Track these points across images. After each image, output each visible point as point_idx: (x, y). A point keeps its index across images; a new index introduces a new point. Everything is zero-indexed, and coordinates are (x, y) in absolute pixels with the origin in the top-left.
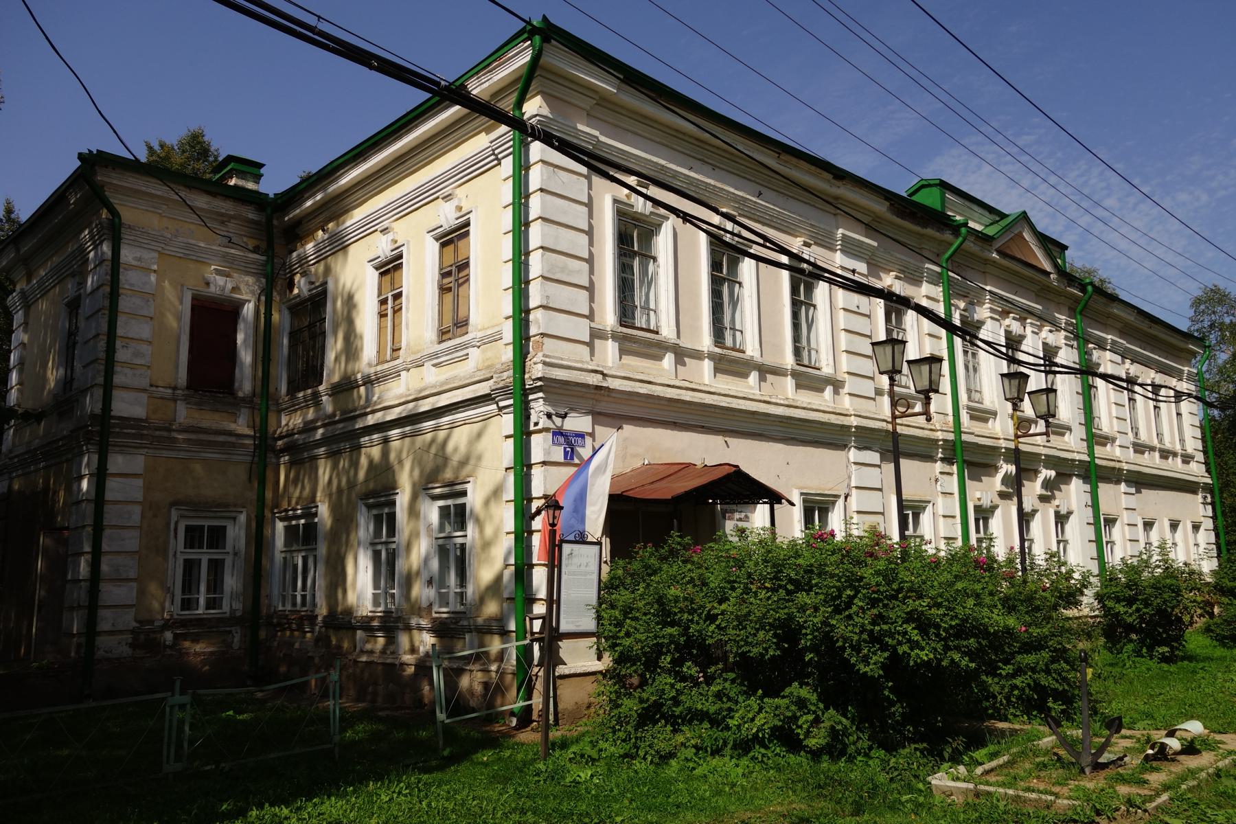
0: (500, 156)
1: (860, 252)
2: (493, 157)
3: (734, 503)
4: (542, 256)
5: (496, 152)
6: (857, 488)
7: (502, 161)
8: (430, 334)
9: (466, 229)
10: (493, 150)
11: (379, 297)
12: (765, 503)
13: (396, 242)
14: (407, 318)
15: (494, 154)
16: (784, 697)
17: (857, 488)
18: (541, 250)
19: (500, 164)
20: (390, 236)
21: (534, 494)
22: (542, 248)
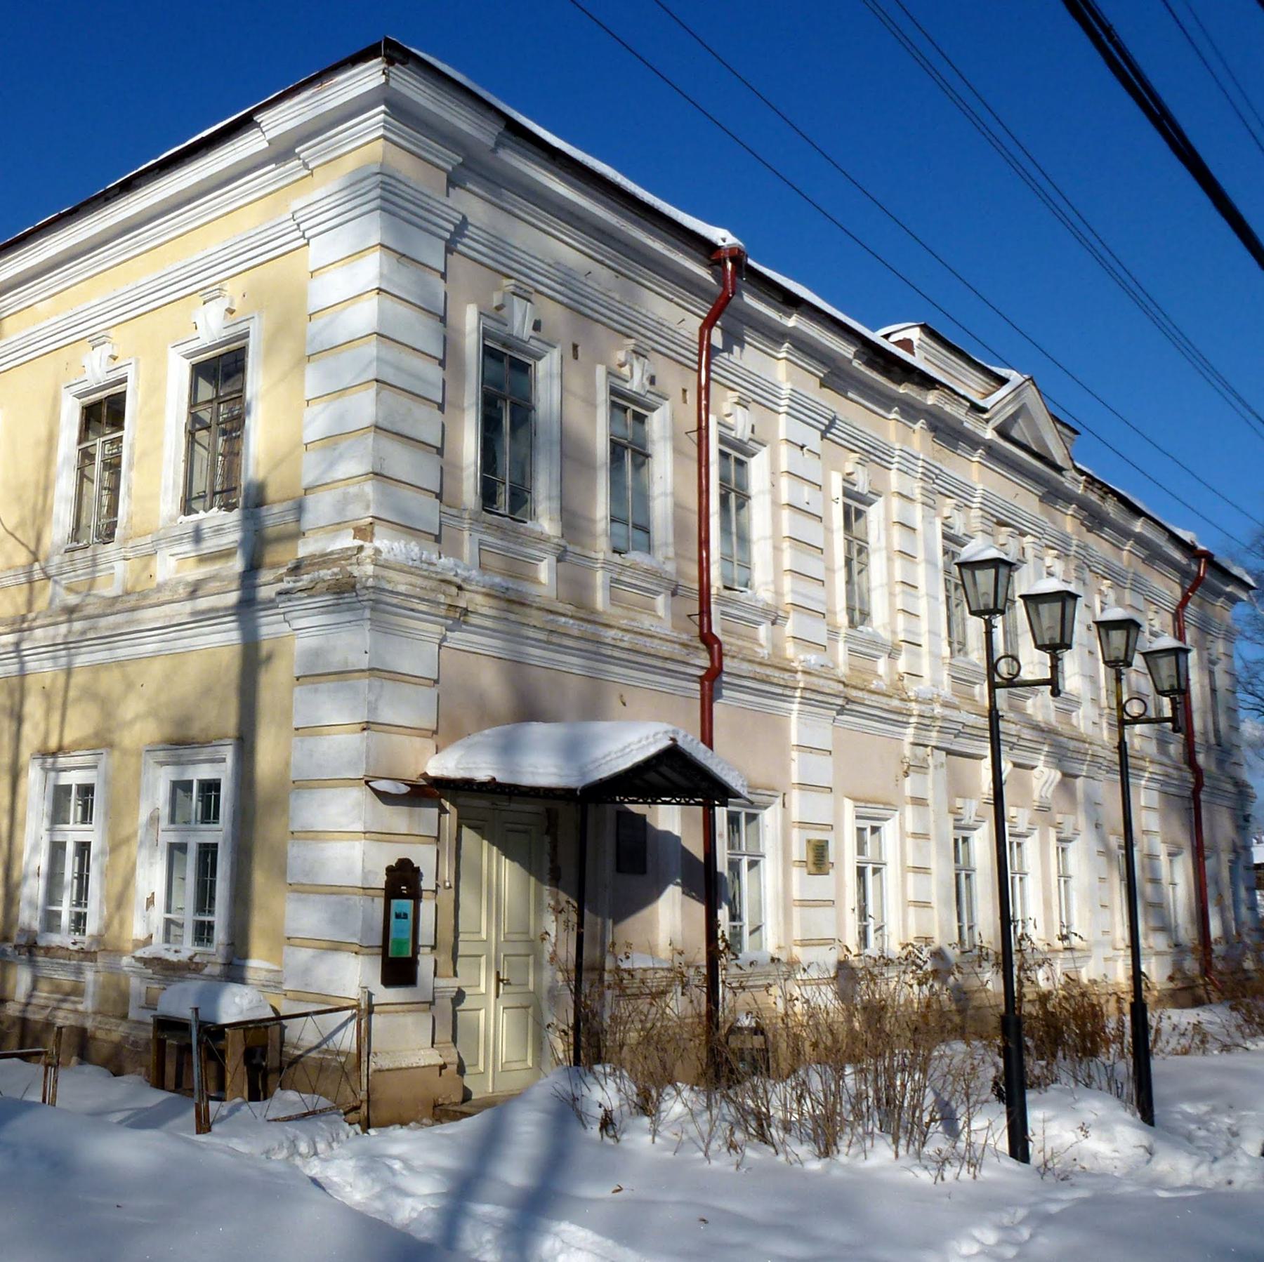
0: (308, 234)
1: (882, 459)
2: (298, 234)
3: (645, 802)
4: (378, 394)
5: (303, 227)
6: (802, 786)
7: (311, 241)
8: (169, 503)
9: (244, 341)
10: (298, 225)
11: (80, 442)
12: (697, 804)
13: (115, 358)
14: (129, 480)
15: (303, 236)
16: (757, 1106)
17: (802, 786)
18: (375, 383)
19: (308, 244)
20: (106, 350)
21: (607, 968)
22: (377, 381)
